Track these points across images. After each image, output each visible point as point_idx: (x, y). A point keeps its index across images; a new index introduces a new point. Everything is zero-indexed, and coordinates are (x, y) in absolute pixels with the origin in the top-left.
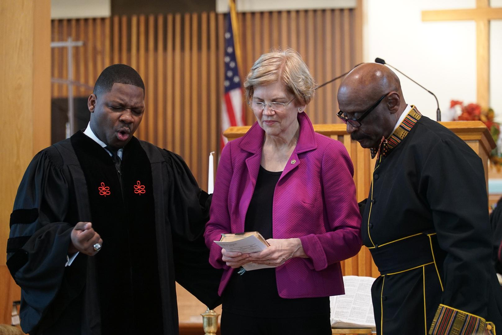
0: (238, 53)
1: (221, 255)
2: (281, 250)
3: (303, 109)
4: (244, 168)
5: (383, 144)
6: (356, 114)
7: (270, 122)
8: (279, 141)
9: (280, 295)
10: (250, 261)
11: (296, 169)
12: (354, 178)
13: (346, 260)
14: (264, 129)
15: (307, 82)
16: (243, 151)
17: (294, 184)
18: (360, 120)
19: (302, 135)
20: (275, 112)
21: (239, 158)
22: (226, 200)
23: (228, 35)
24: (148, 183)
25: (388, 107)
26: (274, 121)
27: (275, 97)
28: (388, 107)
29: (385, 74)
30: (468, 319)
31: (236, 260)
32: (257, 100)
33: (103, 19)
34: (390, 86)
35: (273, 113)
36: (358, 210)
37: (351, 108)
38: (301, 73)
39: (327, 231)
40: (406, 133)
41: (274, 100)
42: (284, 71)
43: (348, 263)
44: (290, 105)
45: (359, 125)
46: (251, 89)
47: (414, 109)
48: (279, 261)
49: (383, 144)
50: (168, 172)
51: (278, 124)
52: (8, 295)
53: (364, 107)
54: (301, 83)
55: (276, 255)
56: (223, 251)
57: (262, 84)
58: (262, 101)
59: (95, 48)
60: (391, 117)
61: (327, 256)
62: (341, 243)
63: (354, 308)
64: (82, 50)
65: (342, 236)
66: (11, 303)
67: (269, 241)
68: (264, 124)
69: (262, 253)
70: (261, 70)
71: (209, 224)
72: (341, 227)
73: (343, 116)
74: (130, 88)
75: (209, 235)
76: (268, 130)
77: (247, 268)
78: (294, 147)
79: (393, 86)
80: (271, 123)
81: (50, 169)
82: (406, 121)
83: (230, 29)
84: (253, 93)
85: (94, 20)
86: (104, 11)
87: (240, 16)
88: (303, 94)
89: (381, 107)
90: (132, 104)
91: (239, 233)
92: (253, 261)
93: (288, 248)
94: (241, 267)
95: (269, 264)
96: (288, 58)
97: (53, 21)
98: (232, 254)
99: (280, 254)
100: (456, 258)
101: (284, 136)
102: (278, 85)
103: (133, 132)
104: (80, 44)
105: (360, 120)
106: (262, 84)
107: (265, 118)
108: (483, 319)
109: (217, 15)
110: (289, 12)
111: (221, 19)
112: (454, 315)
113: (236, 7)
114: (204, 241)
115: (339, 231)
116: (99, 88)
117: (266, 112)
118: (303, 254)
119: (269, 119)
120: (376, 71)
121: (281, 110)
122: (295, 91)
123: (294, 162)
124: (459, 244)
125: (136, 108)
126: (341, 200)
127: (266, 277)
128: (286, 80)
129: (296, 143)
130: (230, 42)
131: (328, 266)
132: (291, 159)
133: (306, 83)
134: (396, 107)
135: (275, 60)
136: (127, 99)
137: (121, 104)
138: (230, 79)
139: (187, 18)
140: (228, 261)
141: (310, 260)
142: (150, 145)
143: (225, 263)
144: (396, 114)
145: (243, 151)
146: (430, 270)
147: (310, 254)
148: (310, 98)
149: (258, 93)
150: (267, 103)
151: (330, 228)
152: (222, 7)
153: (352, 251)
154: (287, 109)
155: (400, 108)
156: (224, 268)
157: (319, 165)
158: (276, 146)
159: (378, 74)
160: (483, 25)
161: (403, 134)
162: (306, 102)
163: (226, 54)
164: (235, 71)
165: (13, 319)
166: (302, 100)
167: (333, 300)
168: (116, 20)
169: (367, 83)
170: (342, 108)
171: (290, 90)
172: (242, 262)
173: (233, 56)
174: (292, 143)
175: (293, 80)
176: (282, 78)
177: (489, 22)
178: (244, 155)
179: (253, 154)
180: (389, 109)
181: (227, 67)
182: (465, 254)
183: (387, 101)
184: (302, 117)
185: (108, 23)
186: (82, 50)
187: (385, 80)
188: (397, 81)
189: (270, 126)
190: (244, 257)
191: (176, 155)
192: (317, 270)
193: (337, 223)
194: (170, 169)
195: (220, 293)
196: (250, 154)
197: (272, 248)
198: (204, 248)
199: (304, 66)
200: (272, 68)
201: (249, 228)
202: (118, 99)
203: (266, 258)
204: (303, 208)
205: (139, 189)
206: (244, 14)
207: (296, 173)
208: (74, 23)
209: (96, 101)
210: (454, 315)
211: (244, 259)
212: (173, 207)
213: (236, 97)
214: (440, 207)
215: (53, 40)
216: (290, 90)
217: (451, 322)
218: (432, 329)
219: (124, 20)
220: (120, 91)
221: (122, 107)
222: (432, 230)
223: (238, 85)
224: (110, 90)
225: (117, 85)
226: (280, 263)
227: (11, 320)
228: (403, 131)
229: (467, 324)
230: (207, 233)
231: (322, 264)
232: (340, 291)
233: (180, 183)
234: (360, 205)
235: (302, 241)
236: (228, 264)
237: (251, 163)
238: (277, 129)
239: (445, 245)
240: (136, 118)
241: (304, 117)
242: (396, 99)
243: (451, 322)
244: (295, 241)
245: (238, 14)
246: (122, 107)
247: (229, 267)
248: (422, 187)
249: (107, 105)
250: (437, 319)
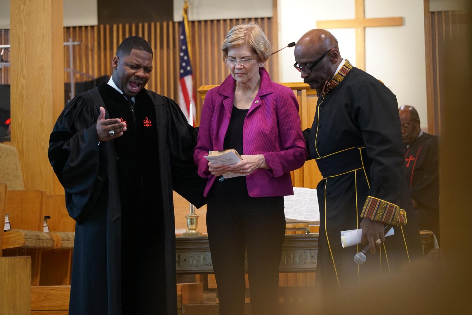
0: (190, 49)
1: (208, 167)
2: (251, 163)
3: (262, 65)
4: (222, 107)
6: (308, 65)
8: (246, 87)
9: (250, 195)
10: (228, 171)
12: (299, 113)
14: (236, 79)
15: (266, 45)
16: (221, 95)
17: (257, 118)
20: (244, 67)
21: (218, 100)
22: (209, 130)
23: (182, 37)
25: (330, 59)
26: (243, 74)
27: (243, 56)
28: (330, 59)
30: (388, 206)
31: (219, 170)
32: (231, 58)
34: (331, 44)
35: (242, 67)
36: (302, 135)
37: (304, 60)
38: (261, 39)
40: (342, 78)
41: (242, 58)
42: (250, 37)
43: (296, 174)
44: (254, 61)
45: (310, 72)
46: (226, 50)
47: (348, 62)
48: (249, 170)
50: (167, 112)
51: (245, 76)
53: (313, 60)
54: (262, 46)
55: (247, 166)
56: (209, 163)
57: (234, 47)
58: (235, 58)
60: (333, 67)
62: (292, 158)
63: (296, 209)
65: (292, 153)
66: (43, 218)
67: (242, 156)
69: (237, 165)
70: (234, 36)
73: (298, 66)
74: (143, 53)
76: (238, 79)
77: (226, 176)
78: (256, 92)
79: (334, 45)
82: (342, 70)
83: (184, 33)
84: (227, 54)
87: (190, 23)
88: (263, 54)
89: (325, 59)
90: (145, 65)
91: (220, 151)
92: (230, 171)
94: (222, 176)
95: (242, 173)
96: (252, 28)
97: (64, 28)
98: (216, 166)
99: (250, 165)
100: (380, 164)
101: (249, 84)
103: (144, 84)
105: (311, 69)
106: (234, 47)
107: (236, 71)
108: (398, 207)
109: (174, 23)
110: (225, 20)
111: (177, 25)
112: (378, 203)
113: (187, 18)
114: (193, 159)
115: (289, 150)
116: (121, 53)
117: (237, 66)
119: (240, 72)
120: (321, 34)
121: (247, 65)
125: (147, 68)
126: (291, 128)
128: (251, 43)
130: (184, 42)
131: (284, 174)
133: (265, 46)
134: (336, 59)
135: (243, 30)
136: (141, 61)
137: (137, 65)
139: (153, 25)
140: (213, 171)
141: (270, 170)
145: (221, 95)
146: (360, 173)
148: (268, 57)
149: (231, 53)
150: (238, 60)
151: (282, 148)
152: (178, 17)
153: (299, 164)
154: (253, 65)
155: (338, 61)
157: (276, 104)
158: (244, 91)
159: (323, 36)
160: (360, 30)
161: (340, 79)
162: (265, 59)
164: (188, 62)
165: (44, 228)
167: (287, 199)
169: (316, 42)
170: (298, 60)
171: (254, 51)
173: (186, 52)
174: (255, 88)
176: (248, 42)
177: (365, 28)
178: (222, 98)
180: (331, 61)
181: (182, 59)
182: (386, 161)
183: (329, 55)
184: (262, 70)
188: (336, 42)
189: (240, 77)
190: (225, 167)
192: (276, 177)
194: (168, 110)
195: (205, 195)
196: (226, 97)
197: (245, 161)
198: (192, 164)
199: (263, 34)
200: (241, 35)
201: (226, 147)
202: (135, 61)
203: (240, 169)
206: (193, 22)
207: (259, 110)
209: (118, 62)
210: (378, 203)
211: (225, 169)
212: (171, 137)
213: (189, 81)
214: (368, 128)
215: (64, 41)
216: (254, 51)
218: (362, 213)
220: (136, 55)
221: (137, 67)
222: (362, 144)
223: (190, 73)
224: (129, 54)
225: (134, 51)
226: (250, 172)
227: (43, 229)
228: (340, 76)
229: (387, 209)
230: (196, 153)
231: (279, 172)
233: (175, 119)
234: (304, 132)
236: (212, 173)
237: (226, 103)
239: (372, 154)
240: (147, 75)
242: (336, 54)
245: (188, 22)
246: (137, 67)
247: (213, 175)
248: (356, 115)
249: (127, 64)
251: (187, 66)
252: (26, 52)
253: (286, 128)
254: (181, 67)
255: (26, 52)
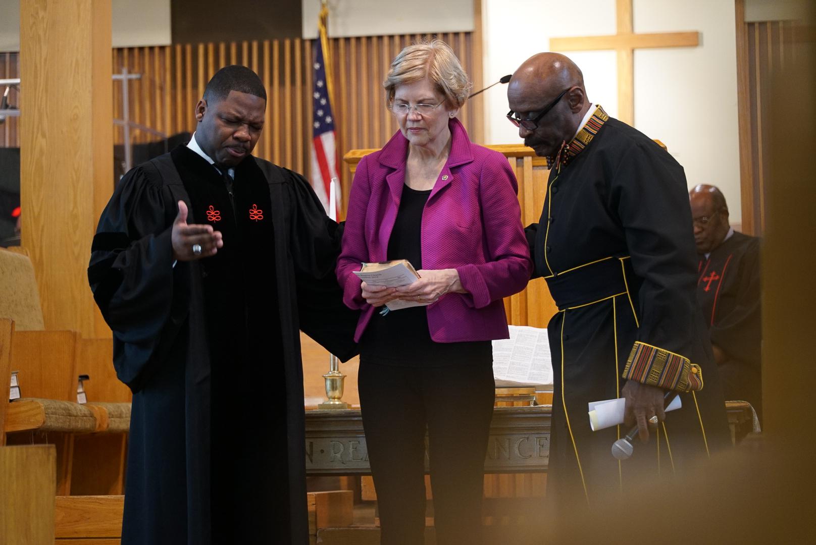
1: (361, 290)
2: (435, 283)
3: (454, 114)
4: (385, 186)
5: (563, 150)
6: (531, 114)
7: (415, 129)
8: (426, 152)
9: (433, 339)
10: (396, 297)
11: (448, 186)
12: (519, 197)
13: (512, 296)
14: (409, 138)
16: (382, 166)
17: (446, 203)
18: (536, 121)
19: (455, 144)
21: (378, 174)
23: (317, 66)
24: (266, 206)
27: (421, 98)
29: (565, 65)
31: (380, 295)
32: (399, 102)
33: (162, 48)
34: (571, 79)
35: (420, 118)
37: (525, 107)
39: (487, 262)
40: (591, 138)
41: (420, 102)
42: (432, 65)
44: (440, 108)
46: (392, 89)
47: (600, 109)
48: (432, 296)
49: (563, 150)
51: (425, 132)
52: (73, 368)
53: (540, 106)
54: (453, 81)
55: (428, 289)
56: (363, 284)
57: (405, 82)
58: (407, 102)
59: (152, 82)
60: (574, 118)
61: (490, 291)
62: (506, 275)
63: (513, 363)
64: (136, 86)
67: (420, 272)
68: (409, 132)
69: (411, 287)
70: (405, 65)
71: (341, 258)
72: (505, 256)
73: (514, 116)
75: (342, 270)
76: (413, 139)
77: (392, 307)
78: (444, 161)
79: (576, 80)
80: (417, 131)
81: (145, 189)
82: (591, 122)
83: (320, 59)
85: (151, 48)
86: (164, 38)
87: (331, 42)
88: (455, 94)
89: (561, 105)
92: (400, 297)
93: (443, 280)
94: (384, 306)
95: (420, 301)
96: (436, 51)
98: (374, 289)
99: (434, 287)
100: (656, 285)
101: (432, 146)
102: (425, 82)
104: (134, 76)
105: (536, 121)
106: (405, 82)
107: (409, 125)
109: (303, 42)
110: (391, 37)
111: (308, 45)
112: (653, 353)
113: (326, 33)
117: (411, 116)
118: (460, 288)
119: (415, 125)
120: (554, 61)
122: (447, 91)
123: (445, 177)
124: (661, 268)
127: (415, 319)
128: (435, 77)
129: (447, 154)
130: (320, 74)
132: (442, 174)
134: (579, 105)
135: (420, 53)
138: (321, 120)
139: (266, 45)
140: (369, 298)
141: (469, 295)
142: (266, 163)
143: (365, 300)
144: (579, 114)
145: (382, 166)
146: (622, 301)
147: (470, 287)
148: (463, 100)
149: (401, 93)
150: (411, 105)
151: (490, 258)
152: (310, 31)
153: (518, 284)
154: (438, 114)
155: (584, 107)
156: (363, 308)
158: (423, 159)
159: (557, 65)
160: (625, 54)
161: (587, 139)
162: (459, 104)
163: (316, 89)
164: (327, 110)
165: (78, 396)
166: (454, 102)
168: (179, 48)
171: (439, 89)
172: (386, 298)
173: (324, 92)
174: (442, 155)
175: (444, 76)
176: (430, 75)
177: (633, 51)
178: (385, 170)
179: (395, 170)
180: (571, 107)
182: (666, 281)
183: (568, 97)
184: (453, 124)
185: (168, 51)
186: (136, 86)
187: (565, 73)
188: (580, 74)
189: (416, 134)
190: (390, 291)
191: (298, 175)
193: (499, 252)
196: (392, 170)
197: (424, 280)
198: (334, 286)
199: (456, 60)
200: (417, 62)
201: (392, 256)
204: (459, 233)
205: (256, 214)
206: (336, 40)
207: (448, 192)
208: (126, 52)
210: (653, 353)
211: (390, 294)
213: (328, 141)
214: (637, 223)
216: (439, 89)
217: (649, 362)
218: (626, 371)
219: (189, 48)
222: (624, 252)
226: (433, 299)
228: (588, 134)
231: (483, 299)
232: (505, 335)
233: (304, 209)
235: (459, 272)
236: (368, 301)
237: (392, 180)
238: (424, 137)
239: (641, 270)
241: (457, 125)
242: (579, 96)
243: (649, 362)
244: (453, 272)
245: (328, 39)
247: (370, 305)
248: (613, 201)
250: (633, 360)
251: (325, 115)
252: (47, 91)
253: (497, 222)
254: (316, 118)
255: (47, 91)
